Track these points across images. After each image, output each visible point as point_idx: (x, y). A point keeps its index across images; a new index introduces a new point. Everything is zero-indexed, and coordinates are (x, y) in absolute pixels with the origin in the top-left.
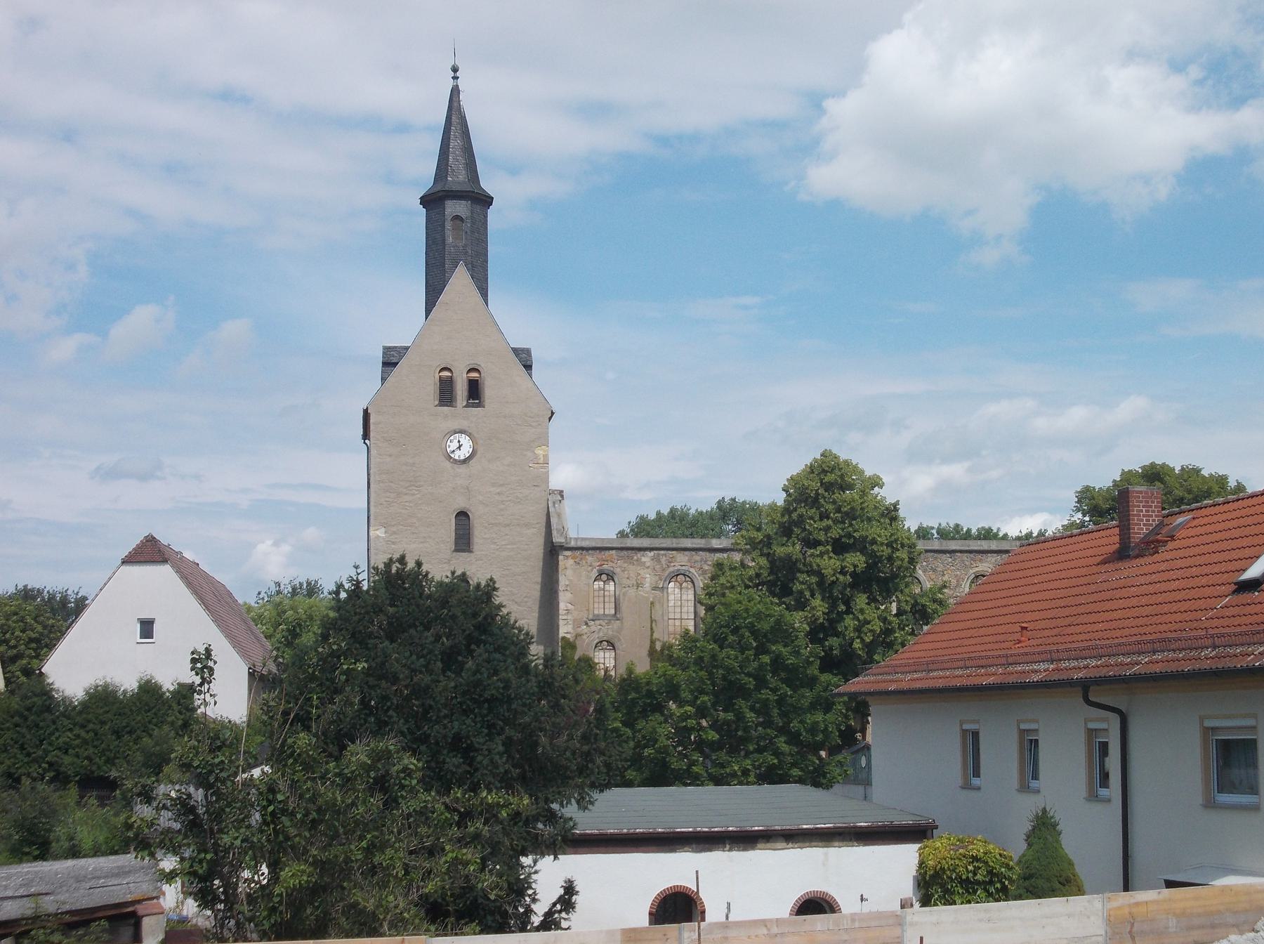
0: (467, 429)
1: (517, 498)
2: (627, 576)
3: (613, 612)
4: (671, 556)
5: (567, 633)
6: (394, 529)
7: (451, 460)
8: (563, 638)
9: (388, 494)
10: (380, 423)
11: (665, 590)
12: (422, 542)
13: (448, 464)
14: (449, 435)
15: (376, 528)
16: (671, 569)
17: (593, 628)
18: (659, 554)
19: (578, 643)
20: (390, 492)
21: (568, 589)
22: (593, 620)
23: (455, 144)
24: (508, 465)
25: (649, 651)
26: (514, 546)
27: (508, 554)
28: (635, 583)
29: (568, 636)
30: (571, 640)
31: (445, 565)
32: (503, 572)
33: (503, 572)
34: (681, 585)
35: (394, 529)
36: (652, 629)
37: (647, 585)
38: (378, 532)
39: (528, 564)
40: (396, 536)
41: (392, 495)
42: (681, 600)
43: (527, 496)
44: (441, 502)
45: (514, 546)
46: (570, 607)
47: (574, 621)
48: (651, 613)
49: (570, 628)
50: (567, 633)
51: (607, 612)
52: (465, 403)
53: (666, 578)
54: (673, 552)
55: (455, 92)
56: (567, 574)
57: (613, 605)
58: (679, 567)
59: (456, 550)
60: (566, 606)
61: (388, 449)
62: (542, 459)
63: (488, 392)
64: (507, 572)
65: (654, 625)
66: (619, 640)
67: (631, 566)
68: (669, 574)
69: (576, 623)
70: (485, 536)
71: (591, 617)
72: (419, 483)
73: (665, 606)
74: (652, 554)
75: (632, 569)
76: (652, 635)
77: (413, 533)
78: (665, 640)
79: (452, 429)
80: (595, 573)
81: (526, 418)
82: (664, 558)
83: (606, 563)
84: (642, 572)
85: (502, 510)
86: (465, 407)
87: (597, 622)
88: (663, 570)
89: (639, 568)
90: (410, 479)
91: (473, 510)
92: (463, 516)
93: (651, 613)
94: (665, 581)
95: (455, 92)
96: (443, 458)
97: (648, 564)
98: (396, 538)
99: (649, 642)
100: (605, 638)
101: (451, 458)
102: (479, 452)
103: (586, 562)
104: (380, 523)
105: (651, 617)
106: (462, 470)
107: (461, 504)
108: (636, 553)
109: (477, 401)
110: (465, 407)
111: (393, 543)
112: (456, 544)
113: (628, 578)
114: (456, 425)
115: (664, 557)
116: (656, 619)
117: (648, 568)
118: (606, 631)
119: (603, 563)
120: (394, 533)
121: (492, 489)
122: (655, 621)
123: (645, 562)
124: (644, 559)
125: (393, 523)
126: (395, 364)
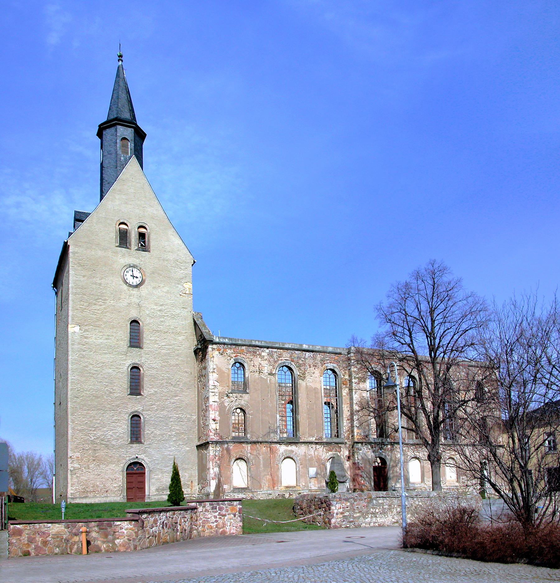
1: (172, 314)
2: (253, 365)
4: (280, 353)
7: (128, 285)
10: (77, 253)
13: (125, 287)
14: (126, 267)
15: (73, 326)
16: (280, 362)
18: (272, 351)
24: (166, 293)
26: (171, 347)
33: (163, 364)
34: (285, 373)
35: (87, 328)
40: (88, 333)
41: (86, 304)
42: (399, 325)
45: (171, 347)
46: (216, 383)
47: (220, 393)
50: (215, 402)
54: (281, 351)
55: (120, 70)
59: (131, 346)
64: (166, 364)
70: (151, 339)
74: (267, 351)
79: (127, 263)
82: (275, 354)
83: (239, 355)
84: (262, 362)
85: (162, 322)
86: (137, 250)
92: (135, 322)
95: (120, 70)
97: (266, 357)
98: (88, 334)
104: (76, 322)
106: (135, 291)
107: (134, 315)
110: (137, 250)
111: (86, 338)
121: (155, 307)
123: (264, 356)
124: (263, 354)
126: (82, 221)
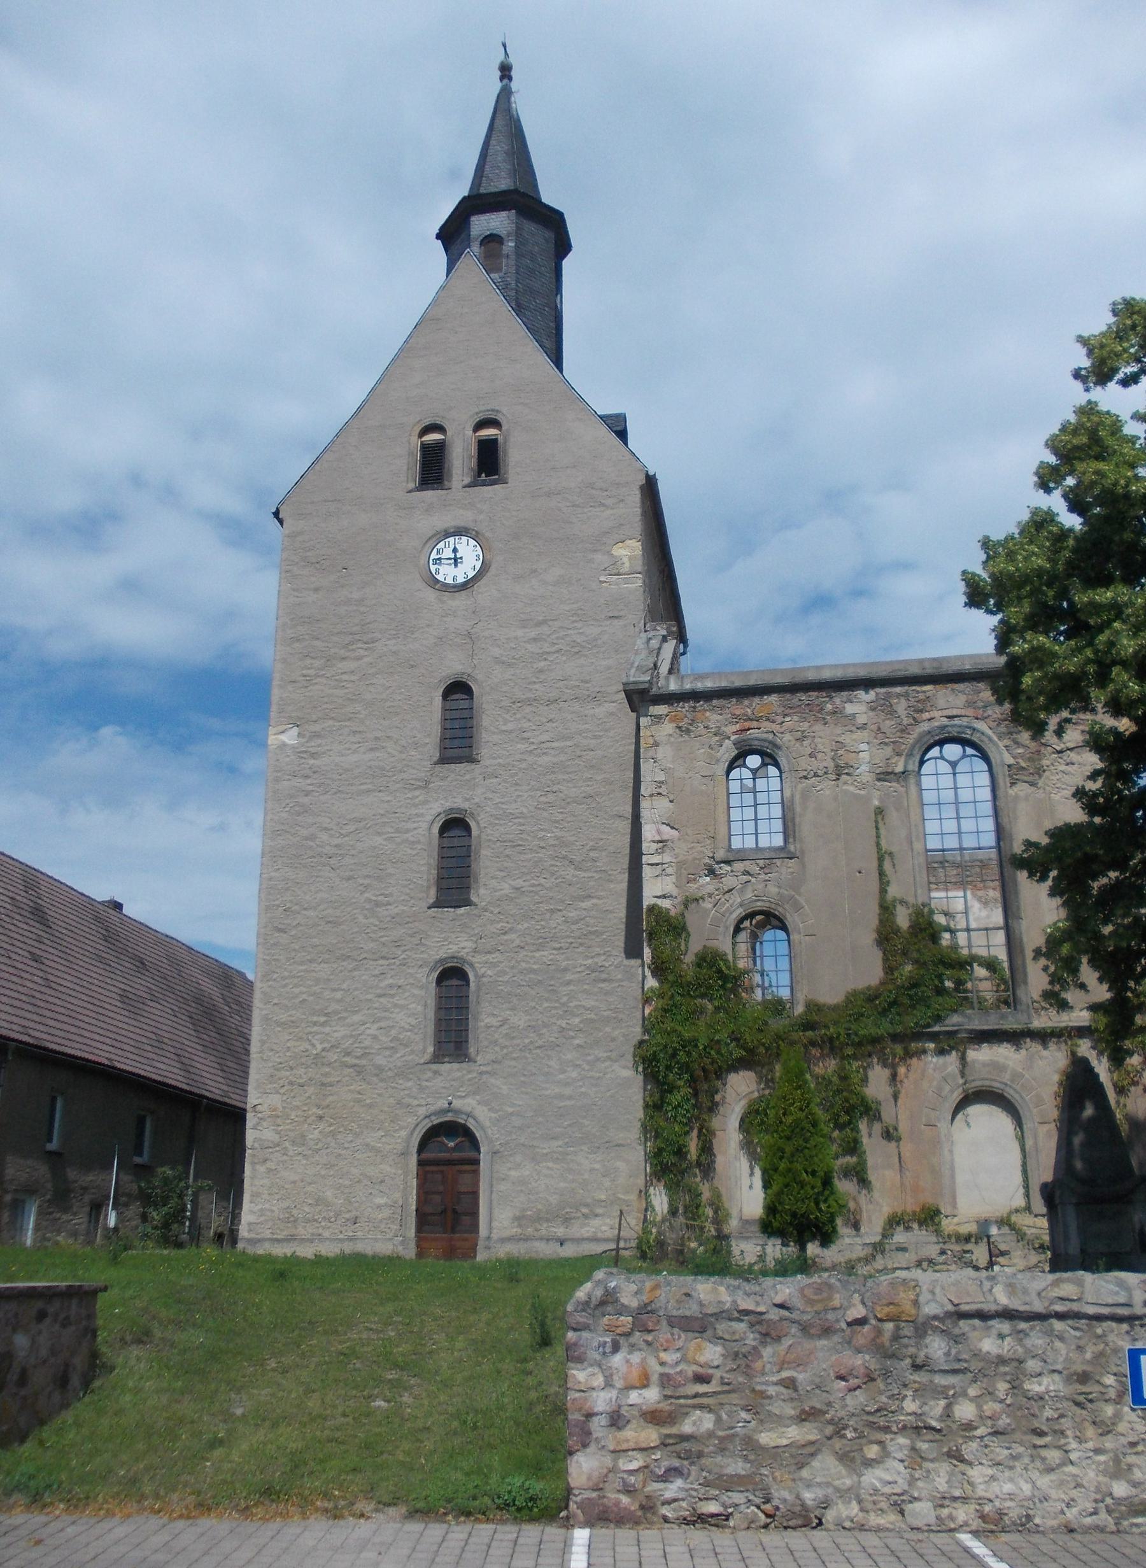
0: (471, 525)
2: (809, 750)
3: (778, 841)
5: (664, 897)
6: (317, 727)
8: (652, 909)
9: (308, 661)
11: (912, 780)
12: (372, 749)
13: (431, 595)
15: (281, 728)
16: (925, 727)
17: (729, 881)
19: (691, 920)
20: (313, 658)
21: (663, 790)
22: (728, 862)
23: (499, 148)
25: (879, 932)
26: (569, 743)
27: (555, 760)
28: (831, 765)
29: (665, 904)
30: (673, 913)
31: (417, 793)
32: (543, 799)
33: (543, 799)
35: (317, 727)
36: (881, 874)
37: (864, 768)
38: (284, 738)
39: (599, 778)
40: (319, 741)
41: (317, 663)
43: (596, 640)
44: (412, 666)
45: (569, 743)
46: (668, 833)
47: (680, 865)
48: (878, 837)
49: (667, 885)
50: (664, 897)
51: (764, 842)
52: (467, 480)
53: (913, 746)
56: (660, 756)
57: (778, 825)
58: (945, 721)
60: (659, 832)
61: (313, 579)
62: (627, 564)
63: (514, 457)
64: (551, 798)
65: (887, 865)
66: (798, 907)
67: (818, 727)
68: (918, 741)
69: (685, 872)
70: (504, 728)
71: (721, 854)
72: (370, 636)
73: (914, 816)
75: (824, 735)
76: (883, 891)
77: (355, 732)
78: (920, 901)
80: (728, 751)
81: (594, 492)
82: (903, 701)
83: (755, 724)
84: (847, 739)
85: (541, 671)
86: (469, 486)
87: (739, 866)
88: (904, 730)
89: (839, 730)
90: (355, 629)
91: (480, 677)
92: (458, 689)
93: (878, 837)
94: (910, 755)
96: (420, 584)
97: (861, 720)
99: (876, 909)
100: (760, 905)
101: (438, 581)
102: (493, 567)
103: (707, 727)
105: (878, 844)
106: (460, 601)
107: (454, 666)
108: (831, 698)
109: (496, 477)
111: (314, 755)
112: (443, 748)
113: (811, 755)
114: (448, 520)
115: (903, 700)
116: (894, 849)
117: (863, 727)
118: (761, 886)
119: (747, 725)
120: (316, 735)
122: (891, 854)
124: (850, 709)
125: (314, 717)
